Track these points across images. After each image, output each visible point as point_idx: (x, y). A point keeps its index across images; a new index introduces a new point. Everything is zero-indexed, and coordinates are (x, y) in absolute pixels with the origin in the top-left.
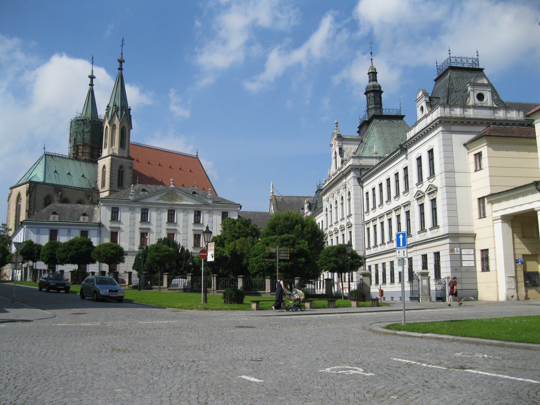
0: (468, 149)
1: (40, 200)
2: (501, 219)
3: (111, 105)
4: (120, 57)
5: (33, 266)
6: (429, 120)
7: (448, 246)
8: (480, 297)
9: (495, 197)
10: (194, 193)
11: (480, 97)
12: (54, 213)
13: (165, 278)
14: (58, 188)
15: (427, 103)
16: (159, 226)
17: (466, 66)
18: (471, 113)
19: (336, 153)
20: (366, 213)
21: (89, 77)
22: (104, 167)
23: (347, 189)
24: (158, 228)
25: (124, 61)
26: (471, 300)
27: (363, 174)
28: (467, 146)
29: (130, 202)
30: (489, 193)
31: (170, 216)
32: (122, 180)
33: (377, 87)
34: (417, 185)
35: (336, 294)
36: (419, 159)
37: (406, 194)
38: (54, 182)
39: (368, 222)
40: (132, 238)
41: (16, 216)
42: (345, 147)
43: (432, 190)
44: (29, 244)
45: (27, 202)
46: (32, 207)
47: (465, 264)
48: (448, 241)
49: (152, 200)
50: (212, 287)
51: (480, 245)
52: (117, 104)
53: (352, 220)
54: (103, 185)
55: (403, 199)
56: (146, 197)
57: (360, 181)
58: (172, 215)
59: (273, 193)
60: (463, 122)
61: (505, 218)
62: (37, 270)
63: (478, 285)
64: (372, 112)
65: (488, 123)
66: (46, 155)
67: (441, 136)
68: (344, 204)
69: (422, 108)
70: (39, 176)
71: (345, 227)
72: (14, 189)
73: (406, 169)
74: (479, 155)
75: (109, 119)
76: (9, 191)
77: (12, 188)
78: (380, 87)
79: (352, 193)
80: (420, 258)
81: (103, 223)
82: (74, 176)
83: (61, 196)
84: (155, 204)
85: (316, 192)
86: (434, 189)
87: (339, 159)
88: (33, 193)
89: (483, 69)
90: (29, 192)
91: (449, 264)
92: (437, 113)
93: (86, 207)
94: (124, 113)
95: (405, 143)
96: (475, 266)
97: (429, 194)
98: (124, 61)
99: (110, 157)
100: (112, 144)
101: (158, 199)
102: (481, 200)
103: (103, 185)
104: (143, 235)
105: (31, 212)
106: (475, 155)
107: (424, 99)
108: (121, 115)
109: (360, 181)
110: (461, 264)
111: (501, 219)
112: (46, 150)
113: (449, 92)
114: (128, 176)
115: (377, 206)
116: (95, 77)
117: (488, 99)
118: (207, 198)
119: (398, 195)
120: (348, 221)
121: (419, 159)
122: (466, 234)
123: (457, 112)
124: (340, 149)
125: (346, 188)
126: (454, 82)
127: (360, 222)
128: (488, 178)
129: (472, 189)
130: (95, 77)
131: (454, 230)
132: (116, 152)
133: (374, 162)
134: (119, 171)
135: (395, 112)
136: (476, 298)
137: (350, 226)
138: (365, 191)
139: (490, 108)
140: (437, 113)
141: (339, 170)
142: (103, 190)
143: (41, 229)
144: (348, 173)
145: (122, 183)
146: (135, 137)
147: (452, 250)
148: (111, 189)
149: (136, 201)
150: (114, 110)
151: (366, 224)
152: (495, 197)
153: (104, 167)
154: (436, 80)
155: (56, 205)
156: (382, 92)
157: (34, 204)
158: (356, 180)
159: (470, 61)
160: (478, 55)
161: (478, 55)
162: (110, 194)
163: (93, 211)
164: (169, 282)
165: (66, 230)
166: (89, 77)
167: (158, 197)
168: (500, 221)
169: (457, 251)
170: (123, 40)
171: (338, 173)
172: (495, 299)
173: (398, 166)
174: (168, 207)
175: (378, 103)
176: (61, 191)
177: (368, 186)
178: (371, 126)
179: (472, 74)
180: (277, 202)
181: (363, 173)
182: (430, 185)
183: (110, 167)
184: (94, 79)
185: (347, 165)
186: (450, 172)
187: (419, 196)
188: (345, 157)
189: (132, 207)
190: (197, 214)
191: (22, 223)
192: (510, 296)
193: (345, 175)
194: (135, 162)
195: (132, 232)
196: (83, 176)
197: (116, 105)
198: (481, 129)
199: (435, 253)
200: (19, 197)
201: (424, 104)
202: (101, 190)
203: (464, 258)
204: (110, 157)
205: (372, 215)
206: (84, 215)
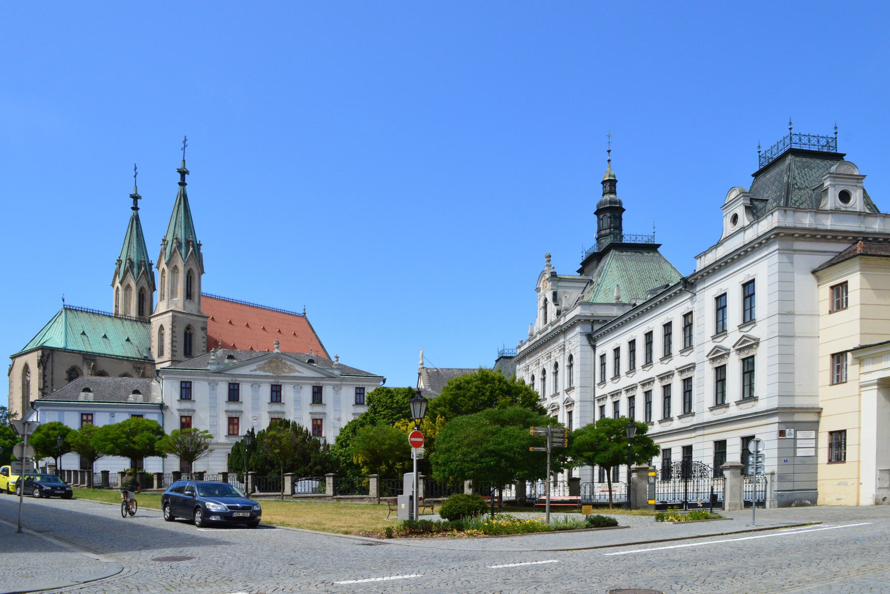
0: (818, 279)
1: (61, 372)
2: (878, 384)
4: (180, 166)
5: (56, 466)
6: (750, 235)
7: (775, 428)
8: (820, 501)
9: (865, 352)
10: (311, 361)
11: (845, 196)
12: (87, 390)
13: (288, 481)
14: (89, 357)
15: (747, 208)
18: (828, 223)
19: (546, 300)
21: (132, 196)
22: (162, 328)
23: (567, 351)
25: (187, 172)
26: (806, 505)
27: (596, 329)
28: (818, 274)
29: (207, 373)
30: (857, 346)
31: (274, 394)
32: (190, 346)
33: (616, 202)
34: (713, 338)
35: (530, 498)
38: (82, 348)
39: (603, 398)
41: (23, 397)
42: (560, 291)
43: (748, 345)
45: (39, 378)
46: (49, 384)
47: (800, 453)
48: (776, 419)
49: (245, 370)
50: (582, 493)
51: (828, 425)
52: (179, 236)
53: (575, 396)
54: (161, 353)
55: (678, 361)
56: (236, 367)
57: (592, 339)
58: (277, 392)
59: (422, 364)
60: (815, 236)
61: (756, 399)
62: (62, 471)
63: (819, 482)
64: (606, 242)
65: (855, 238)
66: (68, 309)
67: (775, 258)
68: (560, 373)
69: (735, 218)
70: (56, 339)
72: (17, 360)
73: (688, 316)
74: (839, 290)
75: (167, 259)
76: (10, 362)
77: (13, 357)
78: (620, 203)
81: (167, 403)
82: (115, 341)
83: (94, 368)
84: (250, 376)
85: (497, 361)
86: (753, 342)
87: (552, 308)
88: (49, 364)
89: (845, 155)
90: (42, 363)
91: (775, 453)
92: (765, 225)
93: (136, 382)
94: (191, 249)
96: (816, 455)
97: (740, 350)
98: (187, 172)
99: (171, 314)
100: (173, 293)
101: (255, 370)
102: (838, 358)
103: (161, 353)
105: (46, 390)
106: (832, 287)
107: (741, 201)
108: (187, 254)
109: (592, 339)
110: (795, 452)
111: (878, 384)
112: (66, 303)
113: (788, 190)
114: (199, 341)
116: (140, 197)
117: (857, 202)
118: (333, 369)
120: (566, 396)
121: (721, 301)
122: (807, 408)
123: (807, 221)
124: (555, 294)
125: (564, 349)
126: (796, 174)
127: (589, 397)
128: (858, 322)
129: (821, 340)
130: (140, 197)
131: (787, 403)
132: (180, 308)
133: (616, 312)
134: (186, 334)
136: (814, 502)
137: (569, 404)
138: (599, 352)
139: (860, 214)
140: (765, 225)
141: (552, 324)
143: (66, 413)
145: (190, 351)
146: (208, 285)
147: (782, 433)
148: (174, 358)
149: (219, 372)
150: (174, 245)
151: (599, 400)
152: (865, 352)
153: (162, 328)
154: (756, 175)
155: (87, 377)
156: (595, 213)
157: (52, 379)
158: (585, 338)
159: (823, 142)
162: (172, 365)
163: (149, 387)
164: (293, 485)
165: (108, 414)
166: (132, 196)
167: (254, 367)
168: (876, 387)
169: (790, 434)
170: (186, 140)
171: (550, 329)
172: (852, 502)
173: (674, 313)
174: (272, 380)
175: (617, 227)
176: (94, 360)
177: (606, 347)
179: (826, 162)
181: (596, 327)
182: (744, 336)
183: (170, 327)
184: (139, 200)
187: (718, 355)
188: (564, 304)
190: (316, 390)
191: (32, 403)
192: (881, 498)
193: (564, 331)
194: (209, 320)
196: (128, 340)
197: (177, 239)
198: (841, 247)
199: (716, 443)
200: (26, 369)
201: (740, 211)
202: (157, 360)
203: (799, 443)
204: (171, 314)
206: (136, 392)
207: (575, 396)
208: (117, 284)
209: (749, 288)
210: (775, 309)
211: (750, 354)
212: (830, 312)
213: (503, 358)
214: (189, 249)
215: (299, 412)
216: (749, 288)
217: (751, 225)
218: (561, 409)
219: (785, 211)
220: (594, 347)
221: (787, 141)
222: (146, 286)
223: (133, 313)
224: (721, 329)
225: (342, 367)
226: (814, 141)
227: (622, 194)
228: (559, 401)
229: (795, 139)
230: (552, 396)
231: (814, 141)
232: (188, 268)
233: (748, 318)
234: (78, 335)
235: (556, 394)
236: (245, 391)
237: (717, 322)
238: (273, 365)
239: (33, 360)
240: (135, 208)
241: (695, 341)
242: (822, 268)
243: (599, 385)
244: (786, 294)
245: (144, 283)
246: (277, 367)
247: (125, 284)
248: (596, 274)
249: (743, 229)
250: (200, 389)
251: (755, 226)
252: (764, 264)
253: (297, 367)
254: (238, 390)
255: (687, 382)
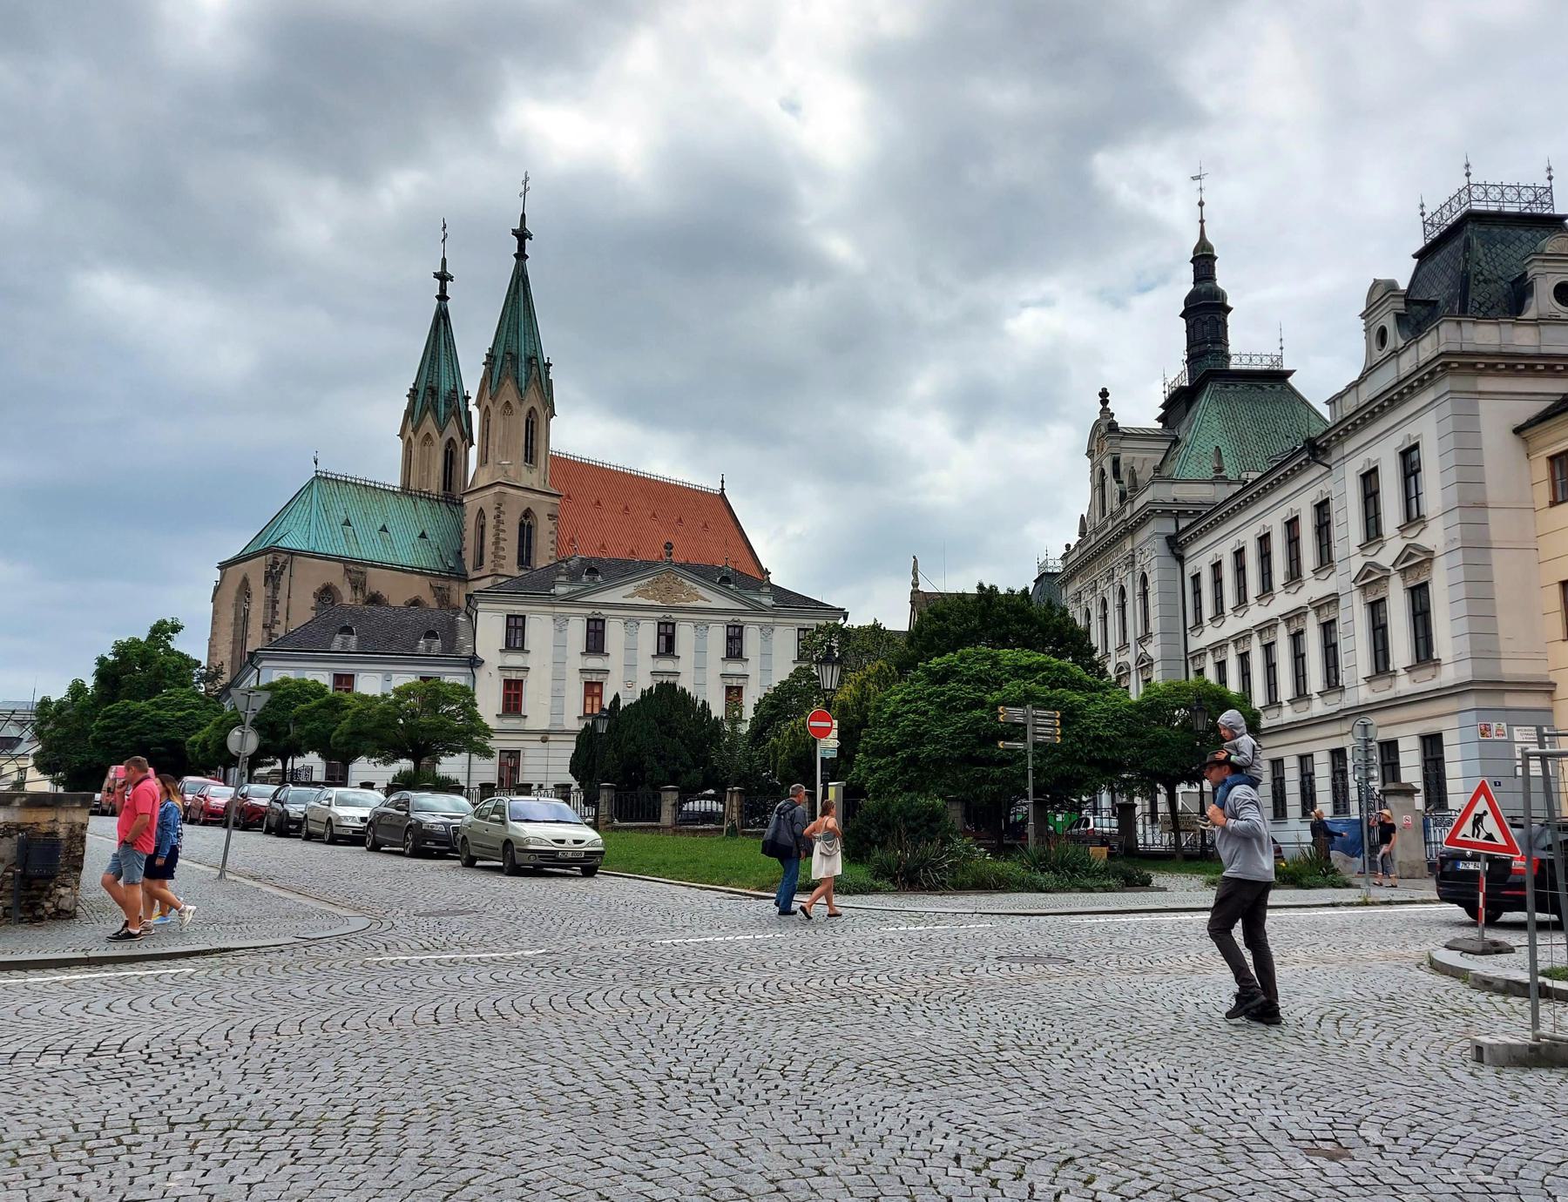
3: (500, 353)
6: (1407, 363)
16: (630, 666)
17: (1510, 209)
20: (1192, 629)
21: (436, 276)
23: (1138, 566)
24: (630, 673)
28: (1526, 434)
32: (529, 548)
34: (1362, 547)
36: (1369, 478)
37: (1323, 576)
38: (343, 551)
39: (1200, 654)
40: (558, 695)
43: (1416, 562)
44: (284, 695)
46: (281, 617)
48: (1471, 702)
53: (1153, 650)
55: (1313, 589)
57: (1176, 547)
60: (1514, 366)
71: (1133, 668)
73: (1322, 508)
77: (223, 566)
79: (1152, 579)
80: (1415, 743)
90: (272, 577)
92: (1427, 348)
95: (1325, 433)
101: (632, 596)
103: (479, 563)
104: (592, 689)
106: (1552, 459)
113: (1464, 283)
115: (1206, 621)
116: (451, 278)
119: (1294, 575)
120: (1141, 651)
121: (1369, 478)
131: (1488, 672)
134: (522, 525)
135: (1267, 361)
138: (1189, 570)
140: (1427, 348)
141: (1113, 516)
142: (477, 574)
144: (1143, 521)
145: (529, 558)
147: (1485, 730)
149: (569, 600)
156: (1229, 310)
159: (1528, 195)
160: (1550, 178)
161: (1550, 178)
165: (380, 676)
166: (436, 276)
167: (629, 589)
170: (527, 179)
173: (1299, 500)
177: (1200, 561)
178: (1203, 400)
180: (981, 587)
181: (1183, 524)
185: (1138, 504)
186: (1473, 506)
187: (1371, 579)
189: (562, 615)
195: (559, 678)
196: (423, 535)
202: (473, 574)
205: (1210, 635)
207: (1153, 650)
208: (409, 433)
209: (1409, 461)
210: (1453, 496)
211: (1422, 580)
212: (1553, 504)
213: (1044, 578)
214: (519, 364)
215: (702, 675)
216: (1409, 461)
217: (1406, 348)
218: (1133, 674)
219: (1459, 323)
220: (1181, 560)
221: (1465, 197)
222: (457, 438)
223: (435, 485)
224: (1373, 531)
225: (779, 592)
226: (1511, 194)
227: (1224, 278)
228: (1129, 658)
229: (1477, 193)
230: (1118, 650)
231: (1511, 194)
232: (446, 437)
233: (1413, 518)
234: (338, 528)
235: (1124, 645)
236: (615, 633)
237: (1367, 520)
238: (662, 586)
239: (256, 571)
240: (443, 297)
241: (1337, 554)
242: (1531, 424)
243: (1192, 629)
244: (1469, 477)
245: (452, 430)
246: (669, 589)
247: (422, 433)
248: (1184, 426)
249: (1396, 353)
250: (539, 627)
251: (1413, 349)
252: (1430, 418)
253: (702, 591)
254: (603, 632)
255: (1328, 628)
